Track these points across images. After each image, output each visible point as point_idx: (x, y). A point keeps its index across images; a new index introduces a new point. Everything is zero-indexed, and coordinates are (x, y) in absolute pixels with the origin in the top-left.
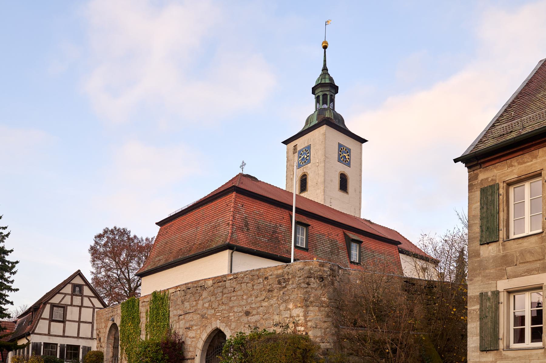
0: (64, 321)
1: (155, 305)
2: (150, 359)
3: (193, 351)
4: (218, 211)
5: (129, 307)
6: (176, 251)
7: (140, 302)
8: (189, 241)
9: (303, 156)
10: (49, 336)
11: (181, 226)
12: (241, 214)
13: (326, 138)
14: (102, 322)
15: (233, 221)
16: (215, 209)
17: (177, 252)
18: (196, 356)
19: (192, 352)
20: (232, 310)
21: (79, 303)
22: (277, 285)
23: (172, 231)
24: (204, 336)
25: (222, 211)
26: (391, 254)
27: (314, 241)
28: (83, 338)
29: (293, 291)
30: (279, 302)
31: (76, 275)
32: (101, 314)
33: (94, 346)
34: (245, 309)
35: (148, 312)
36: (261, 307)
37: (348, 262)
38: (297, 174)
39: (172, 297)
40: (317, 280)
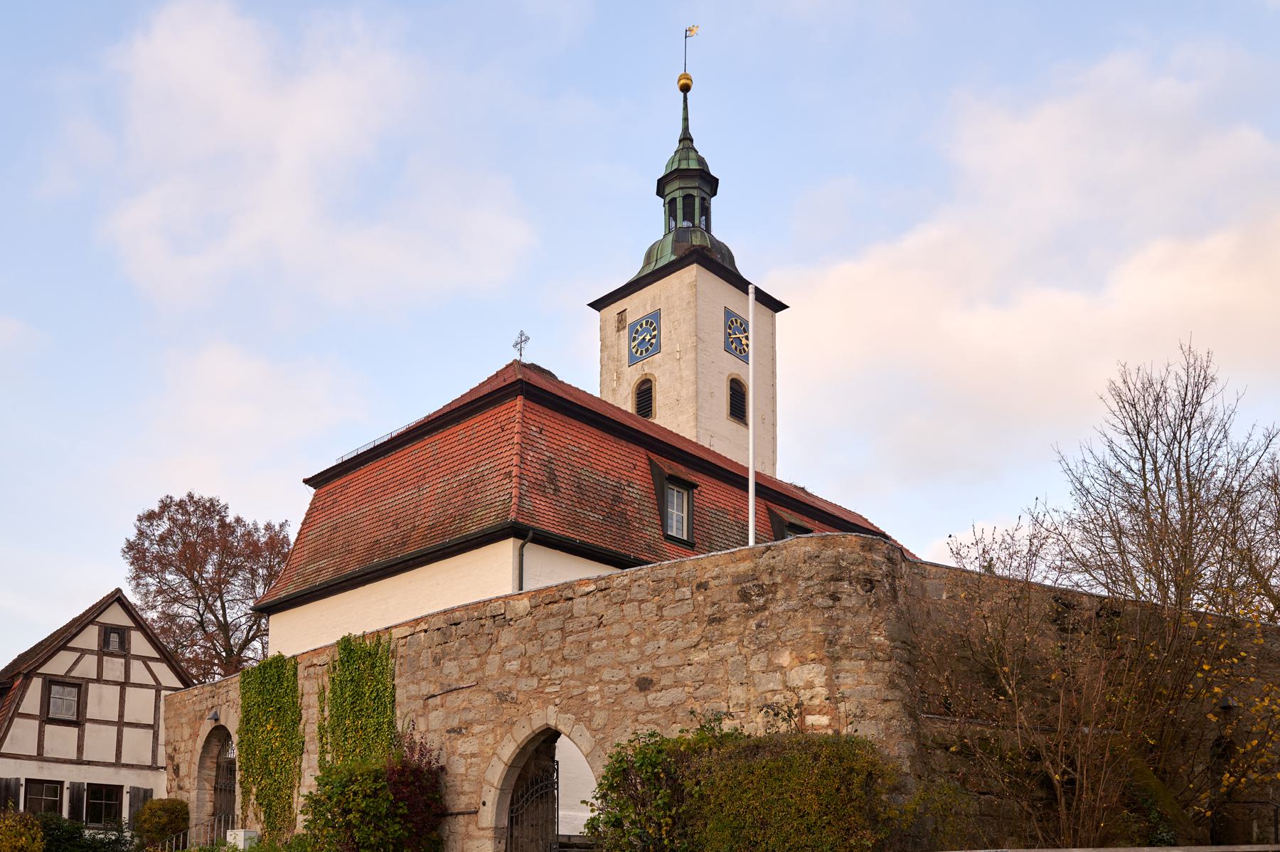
0: (78, 722)
1: (347, 673)
2: (358, 816)
3: (472, 793)
4: (475, 445)
5: (268, 680)
6: (362, 548)
7: (300, 668)
8: (399, 521)
9: (642, 337)
10: (40, 761)
11: (373, 484)
12: (539, 451)
13: (698, 295)
14: (182, 724)
15: (520, 467)
16: (467, 439)
17: (368, 550)
18: (484, 804)
19: (471, 795)
20: (594, 677)
21: (118, 673)
22: (737, 604)
23: (349, 499)
24: (508, 750)
25: (489, 445)
27: (706, 526)
28: (132, 766)
29: (790, 618)
30: (744, 651)
31: (110, 601)
32: (178, 704)
33: (160, 787)
34: (635, 672)
35: (324, 692)
36: (689, 665)
38: (632, 376)
39: (400, 649)
40: (859, 586)
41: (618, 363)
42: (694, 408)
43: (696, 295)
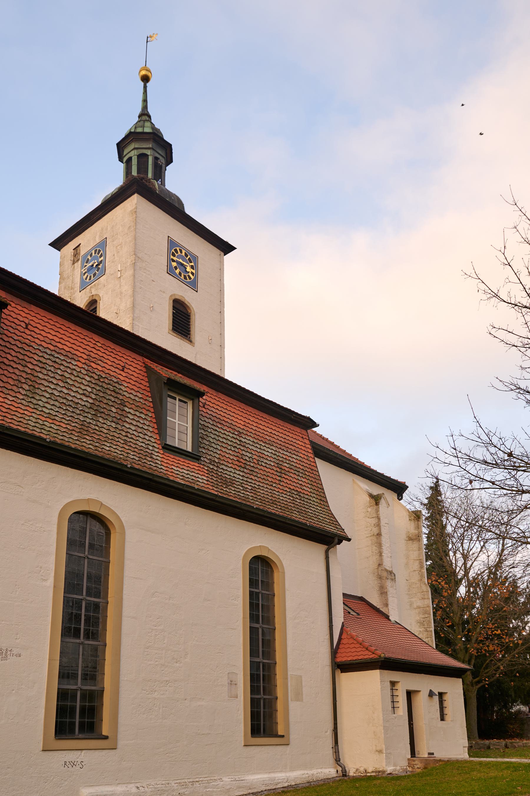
26: (291, 447)
37: (155, 445)
41: (72, 291)
42: (131, 318)
43: (136, 220)
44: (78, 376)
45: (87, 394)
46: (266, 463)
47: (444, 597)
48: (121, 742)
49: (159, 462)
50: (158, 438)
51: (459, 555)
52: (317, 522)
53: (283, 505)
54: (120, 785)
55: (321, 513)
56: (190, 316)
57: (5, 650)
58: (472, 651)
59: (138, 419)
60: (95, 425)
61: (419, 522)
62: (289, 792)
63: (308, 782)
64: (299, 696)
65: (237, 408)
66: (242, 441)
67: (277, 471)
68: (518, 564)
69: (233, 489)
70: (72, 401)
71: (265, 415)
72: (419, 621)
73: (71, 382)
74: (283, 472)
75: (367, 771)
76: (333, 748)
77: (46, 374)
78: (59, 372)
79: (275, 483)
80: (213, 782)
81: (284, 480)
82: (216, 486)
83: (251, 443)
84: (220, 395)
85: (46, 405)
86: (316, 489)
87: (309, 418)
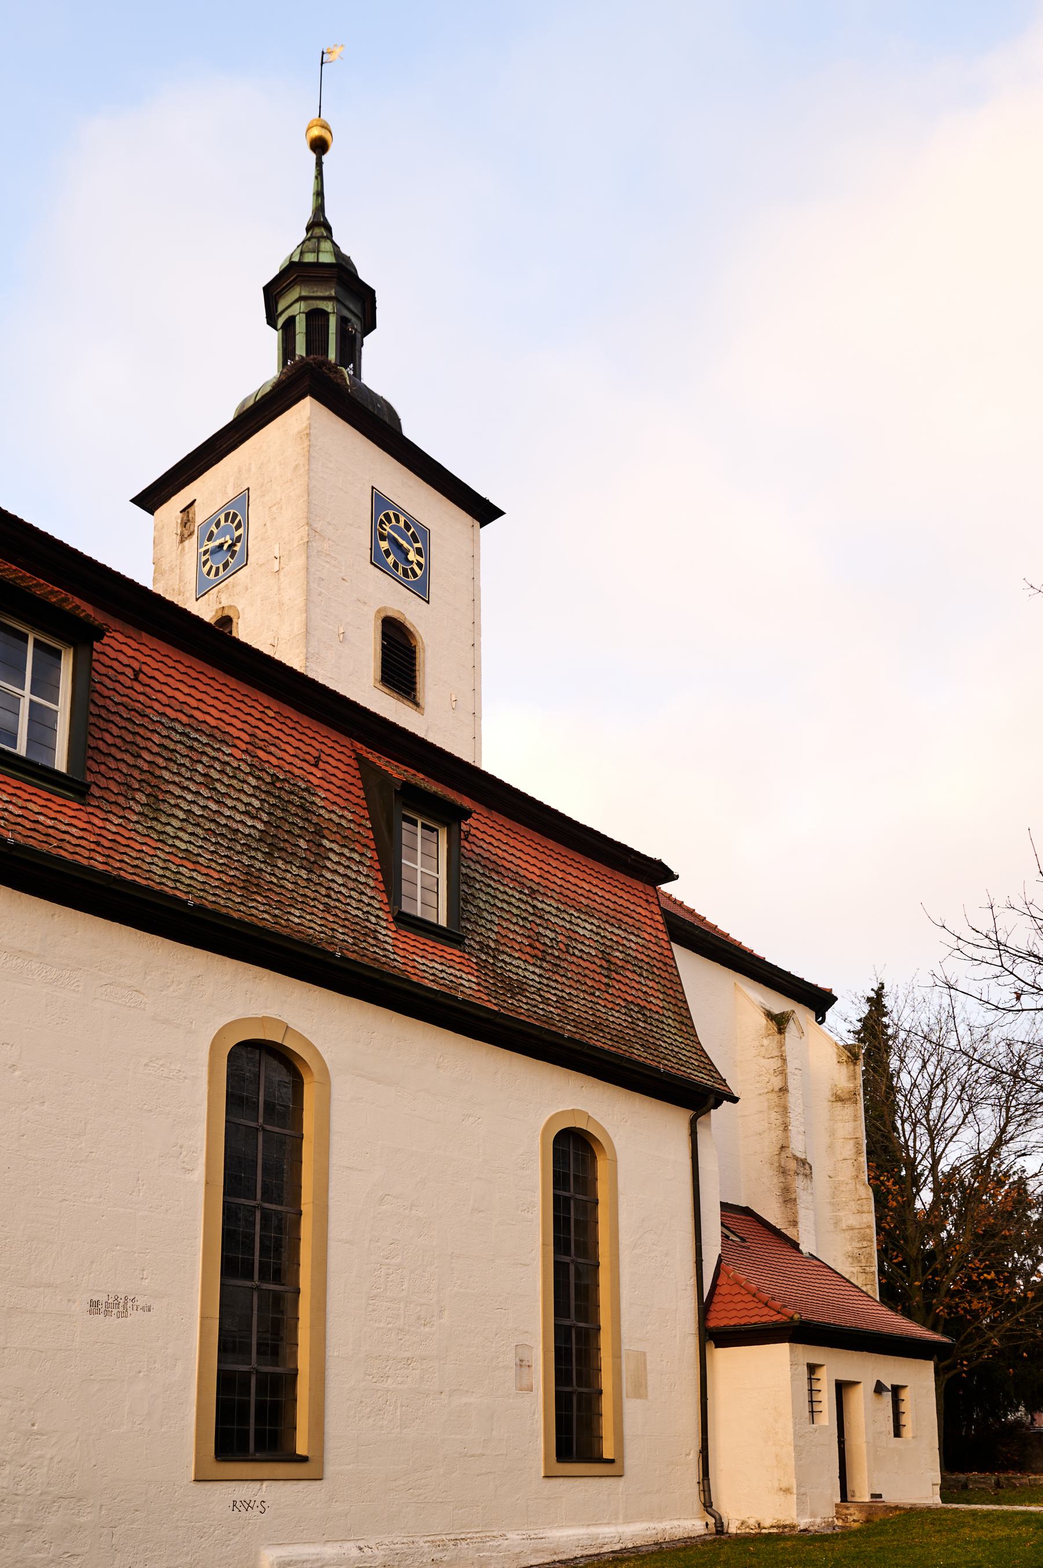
26: (626, 919)
37: (380, 913)
42: (302, 657)
44: (234, 777)
45: (254, 811)
46: (581, 951)
47: (891, 1210)
48: (331, 1468)
49: (390, 948)
50: (386, 901)
51: (921, 1130)
52: (677, 1066)
53: (615, 1033)
54: (331, 1543)
55: (683, 1049)
56: (415, 652)
57: (123, 1299)
58: (940, 1311)
59: (347, 863)
60: (270, 874)
61: (856, 1067)
62: (628, 1559)
63: (656, 1544)
64: (640, 1390)
65: (528, 843)
66: (537, 908)
67: (601, 966)
68: (1034, 1149)
69: (524, 1000)
70: (226, 825)
71: (578, 857)
72: (850, 1254)
73: (223, 789)
74: (612, 967)
75: (762, 1525)
76: (699, 1483)
77: (175, 773)
78: (200, 768)
79: (599, 989)
80: (492, 1540)
81: (615, 984)
82: (494, 994)
83: (554, 911)
84: (495, 815)
85: (180, 834)
86: (674, 1001)
87: (660, 863)
